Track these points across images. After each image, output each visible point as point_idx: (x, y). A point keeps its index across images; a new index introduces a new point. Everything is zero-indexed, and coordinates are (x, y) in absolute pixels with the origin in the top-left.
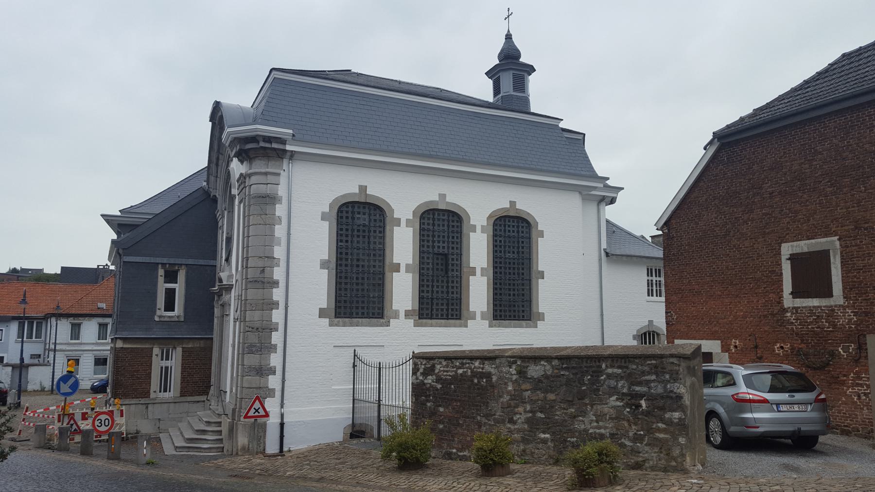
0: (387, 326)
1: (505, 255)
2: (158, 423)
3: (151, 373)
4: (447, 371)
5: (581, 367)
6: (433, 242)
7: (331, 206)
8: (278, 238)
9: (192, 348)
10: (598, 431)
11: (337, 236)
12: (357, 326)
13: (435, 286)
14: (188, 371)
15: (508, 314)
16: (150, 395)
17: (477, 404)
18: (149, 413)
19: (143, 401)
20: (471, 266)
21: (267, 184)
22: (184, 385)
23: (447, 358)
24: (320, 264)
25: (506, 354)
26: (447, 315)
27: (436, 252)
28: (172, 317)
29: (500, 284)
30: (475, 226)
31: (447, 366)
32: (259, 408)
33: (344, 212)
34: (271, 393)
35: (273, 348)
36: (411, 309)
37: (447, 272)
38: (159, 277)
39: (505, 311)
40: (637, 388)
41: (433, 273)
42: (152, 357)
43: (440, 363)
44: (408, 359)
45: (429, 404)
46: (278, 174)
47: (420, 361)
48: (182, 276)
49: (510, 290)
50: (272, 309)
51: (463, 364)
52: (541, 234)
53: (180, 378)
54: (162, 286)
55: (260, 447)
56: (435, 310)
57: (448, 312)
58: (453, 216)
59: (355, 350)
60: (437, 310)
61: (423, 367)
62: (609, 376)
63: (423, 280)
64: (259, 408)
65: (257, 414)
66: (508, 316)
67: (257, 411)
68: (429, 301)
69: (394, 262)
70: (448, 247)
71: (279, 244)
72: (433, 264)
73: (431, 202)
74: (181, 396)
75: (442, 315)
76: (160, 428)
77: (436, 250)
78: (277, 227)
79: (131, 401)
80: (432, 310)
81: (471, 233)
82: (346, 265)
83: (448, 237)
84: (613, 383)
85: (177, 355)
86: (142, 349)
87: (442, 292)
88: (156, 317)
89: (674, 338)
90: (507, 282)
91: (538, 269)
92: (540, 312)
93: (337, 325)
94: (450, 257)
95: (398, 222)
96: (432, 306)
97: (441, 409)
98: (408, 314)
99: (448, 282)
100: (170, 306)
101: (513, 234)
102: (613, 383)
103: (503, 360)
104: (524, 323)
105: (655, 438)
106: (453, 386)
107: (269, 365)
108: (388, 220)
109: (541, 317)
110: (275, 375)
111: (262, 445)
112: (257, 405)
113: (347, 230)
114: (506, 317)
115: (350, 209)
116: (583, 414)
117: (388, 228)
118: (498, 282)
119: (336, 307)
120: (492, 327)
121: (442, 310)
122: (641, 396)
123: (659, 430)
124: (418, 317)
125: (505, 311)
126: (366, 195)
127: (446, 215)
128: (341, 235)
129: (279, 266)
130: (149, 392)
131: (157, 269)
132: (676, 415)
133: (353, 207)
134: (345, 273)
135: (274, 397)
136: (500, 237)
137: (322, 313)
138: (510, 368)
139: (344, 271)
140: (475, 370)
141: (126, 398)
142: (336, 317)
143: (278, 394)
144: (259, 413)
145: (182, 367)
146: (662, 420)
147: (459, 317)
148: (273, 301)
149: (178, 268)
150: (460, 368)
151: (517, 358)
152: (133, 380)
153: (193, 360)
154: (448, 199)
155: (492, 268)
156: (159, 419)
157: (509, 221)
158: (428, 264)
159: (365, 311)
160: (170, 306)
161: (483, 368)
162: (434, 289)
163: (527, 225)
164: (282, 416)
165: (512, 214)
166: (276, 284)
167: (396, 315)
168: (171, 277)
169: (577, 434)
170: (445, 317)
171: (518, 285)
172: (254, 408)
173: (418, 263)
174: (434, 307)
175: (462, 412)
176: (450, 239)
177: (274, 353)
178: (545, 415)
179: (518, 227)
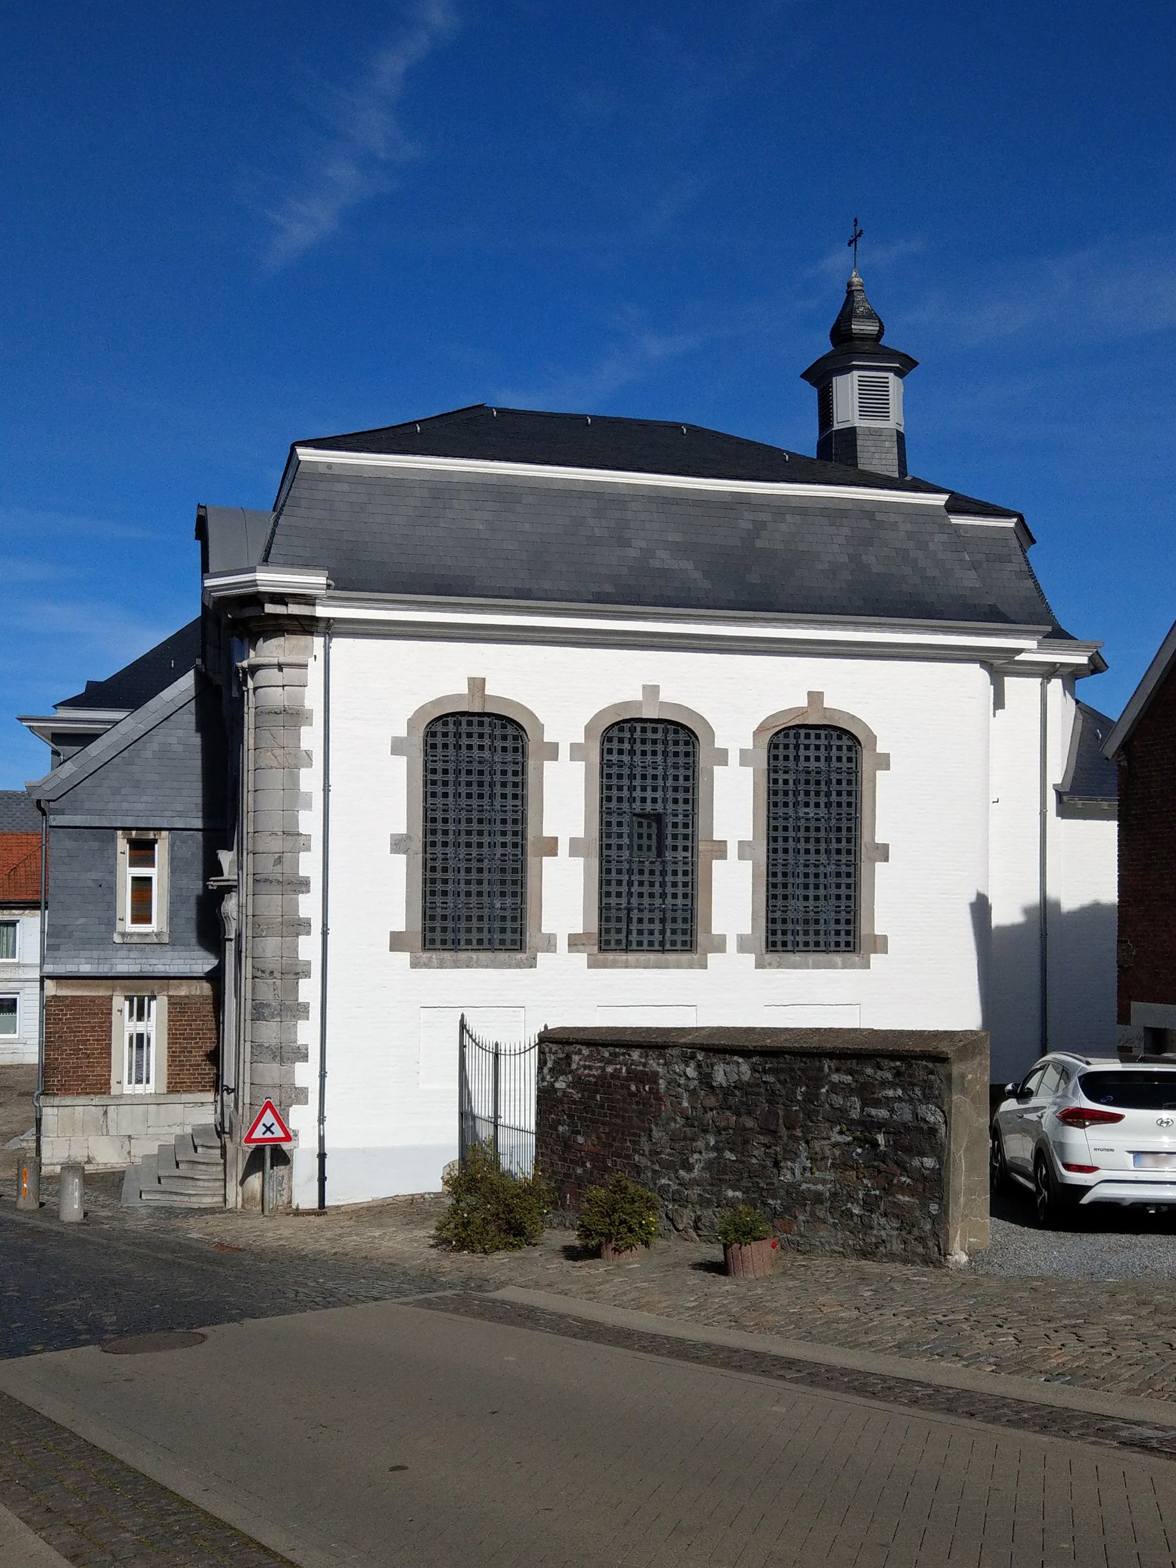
0: (531, 967)
1: (796, 813)
2: (127, 1142)
3: (110, 1044)
4: (590, 1068)
5: (793, 1070)
6: (632, 788)
7: (411, 723)
8: (307, 794)
9: (186, 996)
10: (813, 1187)
11: (425, 785)
12: (468, 967)
13: (636, 883)
14: (180, 1043)
15: (801, 938)
16: (110, 1088)
17: (635, 1131)
18: (110, 1123)
19: (97, 1100)
20: (714, 839)
21: (283, 686)
22: (173, 1070)
23: (588, 1043)
24: (391, 844)
25: (682, 1040)
26: (662, 943)
27: (638, 811)
28: (147, 935)
29: (785, 875)
30: (725, 752)
31: (590, 1057)
32: (273, 1124)
33: (439, 735)
34: (300, 1096)
35: (302, 1011)
36: (581, 932)
37: (660, 854)
38: (119, 856)
39: (795, 933)
40: (873, 1112)
41: (631, 855)
42: (111, 1014)
43: (579, 1052)
44: (533, 1044)
45: (560, 1128)
46: (305, 666)
47: (548, 1046)
48: (161, 852)
49: (806, 887)
50: (297, 935)
51: (616, 1055)
52: (884, 762)
53: (166, 1057)
54: (127, 873)
55: (282, 1195)
56: (635, 933)
57: (664, 938)
58: (676, 732)
59: (463, 1016)
60: (640, 932)
61: (553, 1057)
62: (835, 1088)
63: (609, 871)
64: (273, 1124)
65: (268, 1135)
66: (801, 944)
67: (268, 1129)
68: (623, 914)
69: (545, 835)
70: (665, 800)
71: (308, 806)
72: (630, 836)
73: (626, 705)
74: (169, 1092)
75: (651, 943)
76: (132, 1154)
77: (637, 806)
78: (303, 772)
79: (76, 1099)
80: (629, 932)
81: (715, 767)
82: (445, 844)
83: (665, 778)
84: (838, 1100)
85: (158, 1009)
86: (93, 999)
87: (651, 895)
88: (115, 935)
89: (1130, 998)
90: (801, 869)
91: (873, 839)
92: (876, 933)
93: (427, 965)
94: (670, 820)
95: (552, 751)
96: (628, 926)
97: (580, 1139)
98: (575, 943)
99: (663, 873)
100: (142, 914)
101: (817, 764)
102: (838, 1100)
103: (675, 1052)
104: (838, 958)
105: (895, 1202)
106: (598, 1097)
107: (295, 1042)
108: (531, 747)
109: (880, 945)
110: (307, 1061)
111: (285, 1193)
112: (268, 1118)
113: (445, 772)
114: (798, 945)
115: (451, 728)
116: (793, 1156)
117: (531, 764)
118: (779, 870)
119: (424, 929)
120: (763, 967)
121: (651, 933)
122: (879, 1125)
123: (902, 1188)
124: (596, 948)
125: (795, 933)
126: (484, 697)
127: (660, 731)
128: (434, 783)
129: (308, 849)
130: (108, 1083)
131: (114, 839)
132: (929, 1162)
133: (458, 724)
134: (443, 859)
135: (306, 1103)
136: (786, 772)
137: (397, 942)
138: (687, 1066)
139: (440, 855)
140: (633, 1067)
141: (65, 1094)
142: (425, 948)
143: (314, 1097)
144: (273, 1133)
145: (169, 1034)
146: (905, 1170)
147: (689, 946)
148: (300, 919)
149: (155, 835)
150: (609, 1062)
151: (697, 1049)
152: (77, 1058)
153: (188, 1020)
154: (664, 696)
155: (765, 842)
156: (129, 1137)
157: (807, 736)
158: (620, 836)
159: (485, 936)
160: (142, 914)
161: (645, 1065)
162: (633, 890)
163: (850, 743)
164: (322, 1139)
165: (812, 720)
166: (303, 885)
167: (549, 944)
168: (142, 850)
169: (782, 1192)
170: (657, 947)
171: (825, 877)
172: (264, 1125)
173: (597, 835)
174: (634, 926)
175: (611, 1146)
176: (670, 783)
177: (304, 1019)
178: (736, 1157)
179: (828, 747)
